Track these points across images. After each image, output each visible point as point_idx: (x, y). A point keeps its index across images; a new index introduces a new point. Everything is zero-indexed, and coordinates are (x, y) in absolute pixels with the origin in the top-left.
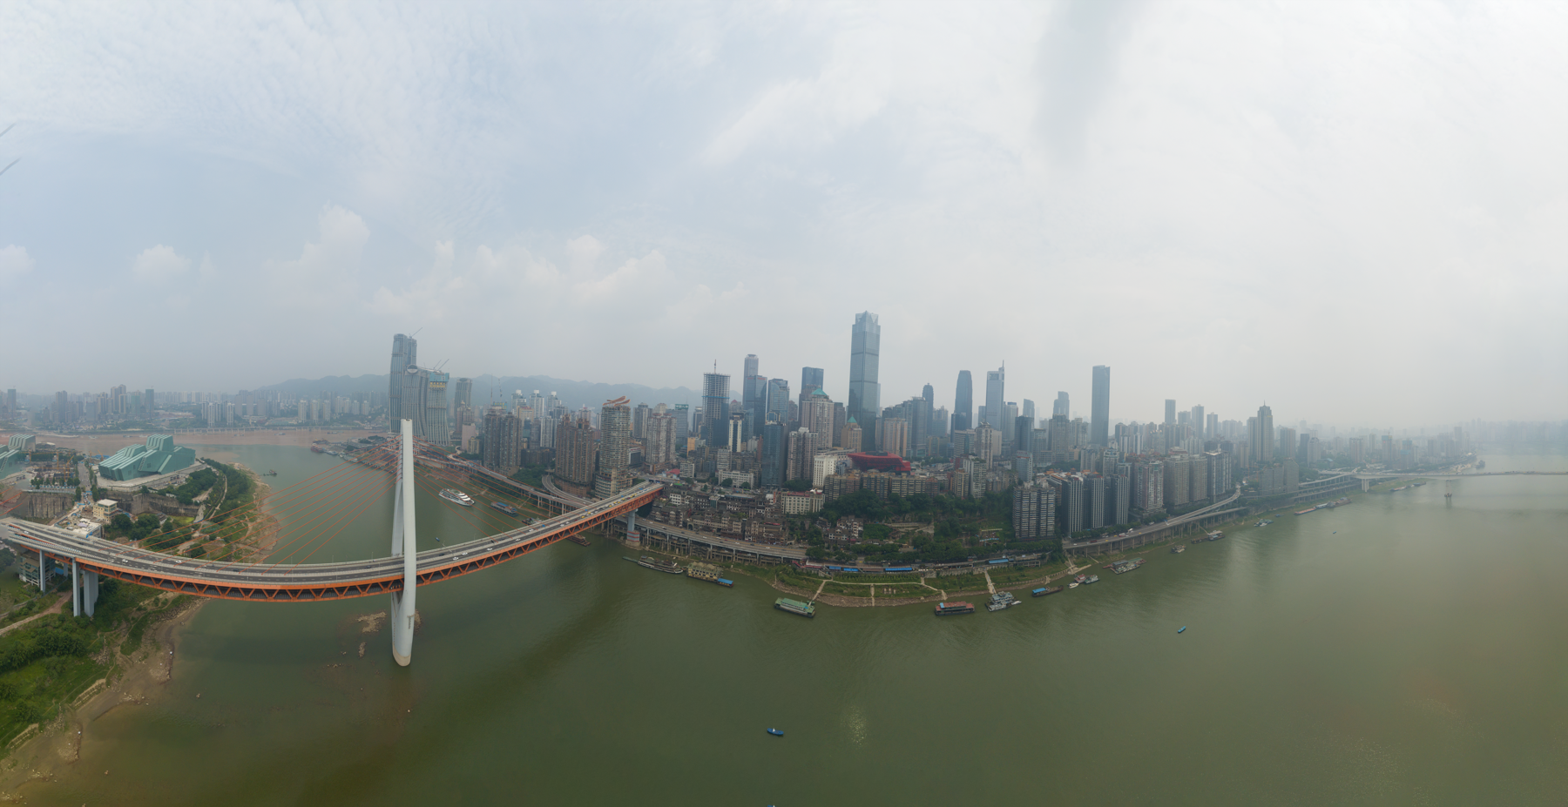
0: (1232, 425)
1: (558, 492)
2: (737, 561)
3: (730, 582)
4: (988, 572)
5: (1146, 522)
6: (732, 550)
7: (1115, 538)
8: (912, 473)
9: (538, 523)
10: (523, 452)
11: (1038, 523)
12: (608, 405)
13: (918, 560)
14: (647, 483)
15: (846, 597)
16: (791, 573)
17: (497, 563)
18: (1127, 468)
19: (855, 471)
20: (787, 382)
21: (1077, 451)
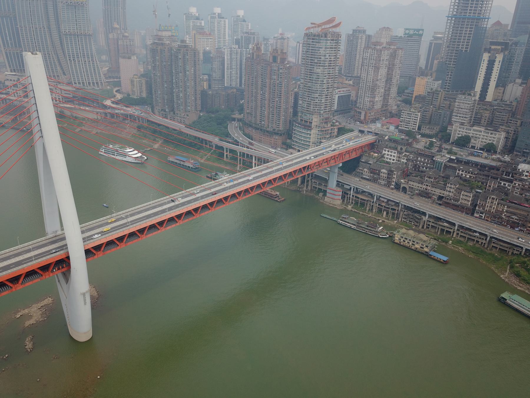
2: (459, 238)
3: (445, 258)
6: (454, 224)
10: (204, 93)
12: (312, 31)
14: (356, 133)
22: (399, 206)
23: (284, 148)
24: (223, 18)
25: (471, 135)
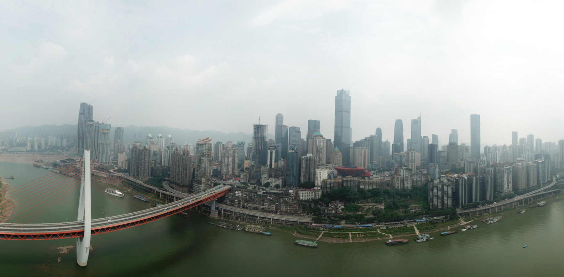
0: (549, 144)
1: (171, 190)
2: (273, 224)
3: (270, 233)
4: (416, 225)
5: (503, 199)
6: (270, 219)
7: (486, 207)
8: (371, 177)
9: (160, 206)
10: (152, 168)
11: (443, 201)
12: (199, 142)
13: (376, 221)
14: (222, 185)
15: (335, 239)
16: (304, 229)
17: (137, 225)
18: (492, 170)
19: (339, 177)
20: (299, 128)
21: (463, 162)
22: (245, 215)
23: (189, 193)
24: (162, 138)
25: (269, 182)
